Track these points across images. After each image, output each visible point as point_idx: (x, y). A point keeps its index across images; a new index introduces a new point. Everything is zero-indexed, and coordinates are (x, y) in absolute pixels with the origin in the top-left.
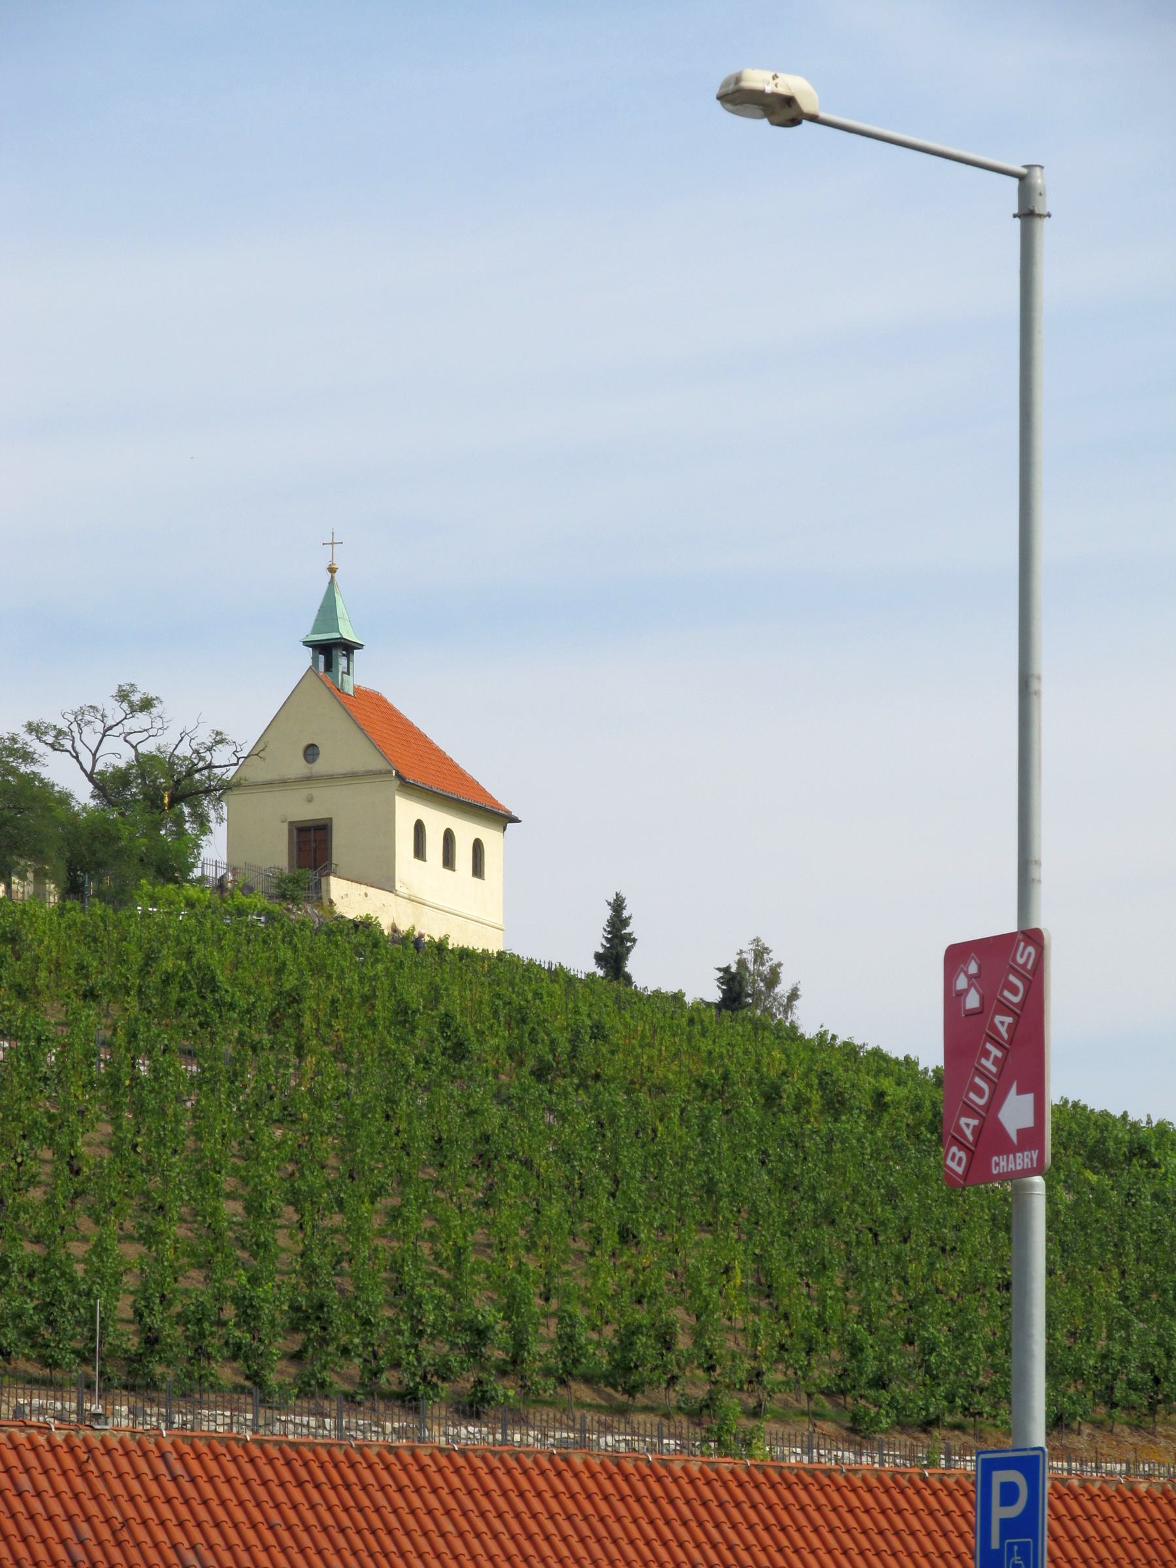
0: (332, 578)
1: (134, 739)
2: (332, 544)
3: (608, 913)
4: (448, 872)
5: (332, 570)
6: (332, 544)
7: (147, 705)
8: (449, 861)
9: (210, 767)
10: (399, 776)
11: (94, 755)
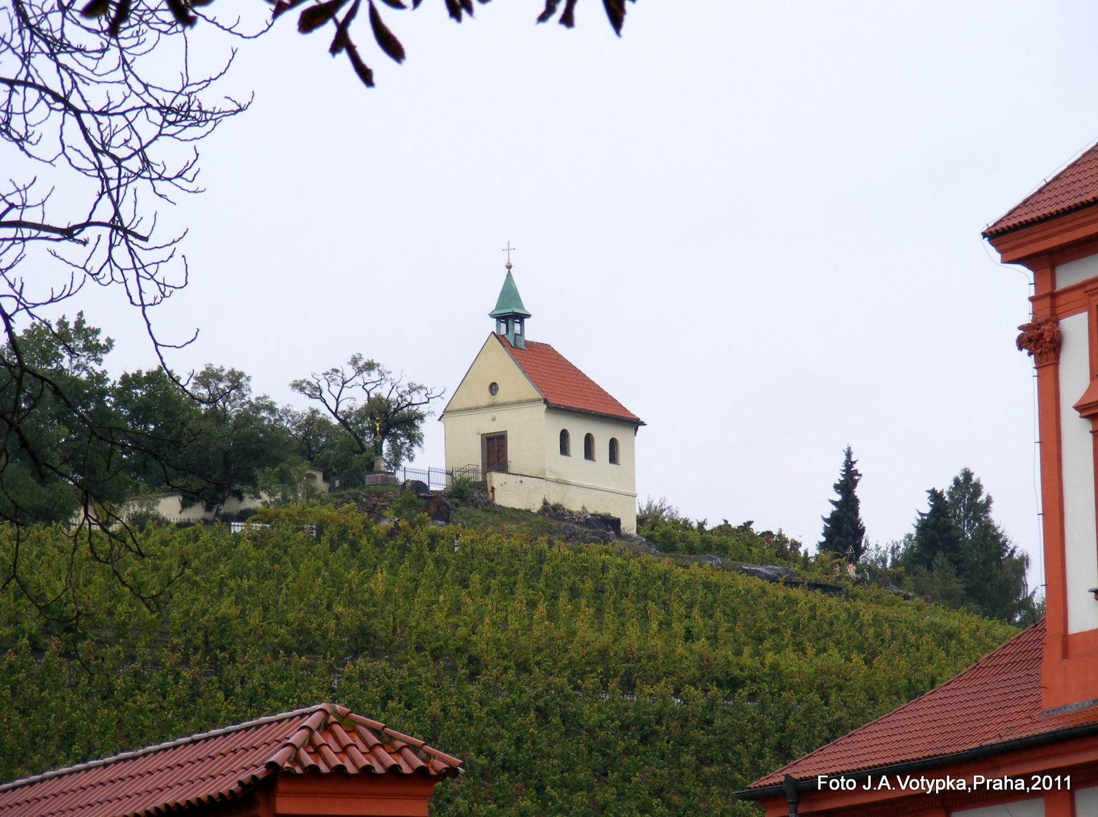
0: (509, 272)
1: (368, 387)
2: (509, 250)
3: (844, 458)
4: (589, 462)
5: (509, 267)
6: (509, 250)
7: (370, 366)
8: (589, 453)
9: (410, 404)
10: (546, 402)
11: (337, 400)
